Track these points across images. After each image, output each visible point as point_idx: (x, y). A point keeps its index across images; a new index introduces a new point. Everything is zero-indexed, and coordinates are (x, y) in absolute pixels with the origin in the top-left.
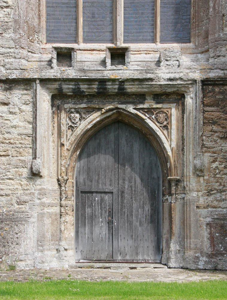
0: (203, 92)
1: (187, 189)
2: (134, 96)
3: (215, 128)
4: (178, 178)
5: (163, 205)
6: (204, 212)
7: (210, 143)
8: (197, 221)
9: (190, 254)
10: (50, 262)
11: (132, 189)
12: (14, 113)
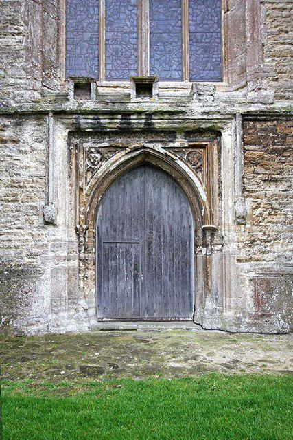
0: (243, 129)
1: (226, 238)
2: (163, 135)
3: (258, 169)
4: (215, 226)
5: (196, 259)
6: (247, 265)
7: (252, 186)
8: (238, 276)
9: (229, 314)
10: (67, 324)
11: (160, 240)
12: (25, 152)
